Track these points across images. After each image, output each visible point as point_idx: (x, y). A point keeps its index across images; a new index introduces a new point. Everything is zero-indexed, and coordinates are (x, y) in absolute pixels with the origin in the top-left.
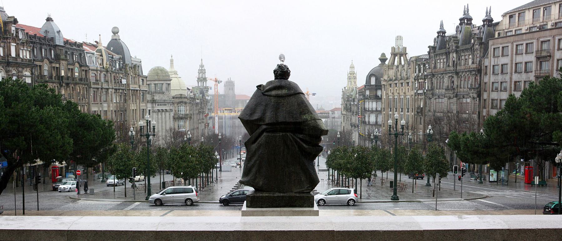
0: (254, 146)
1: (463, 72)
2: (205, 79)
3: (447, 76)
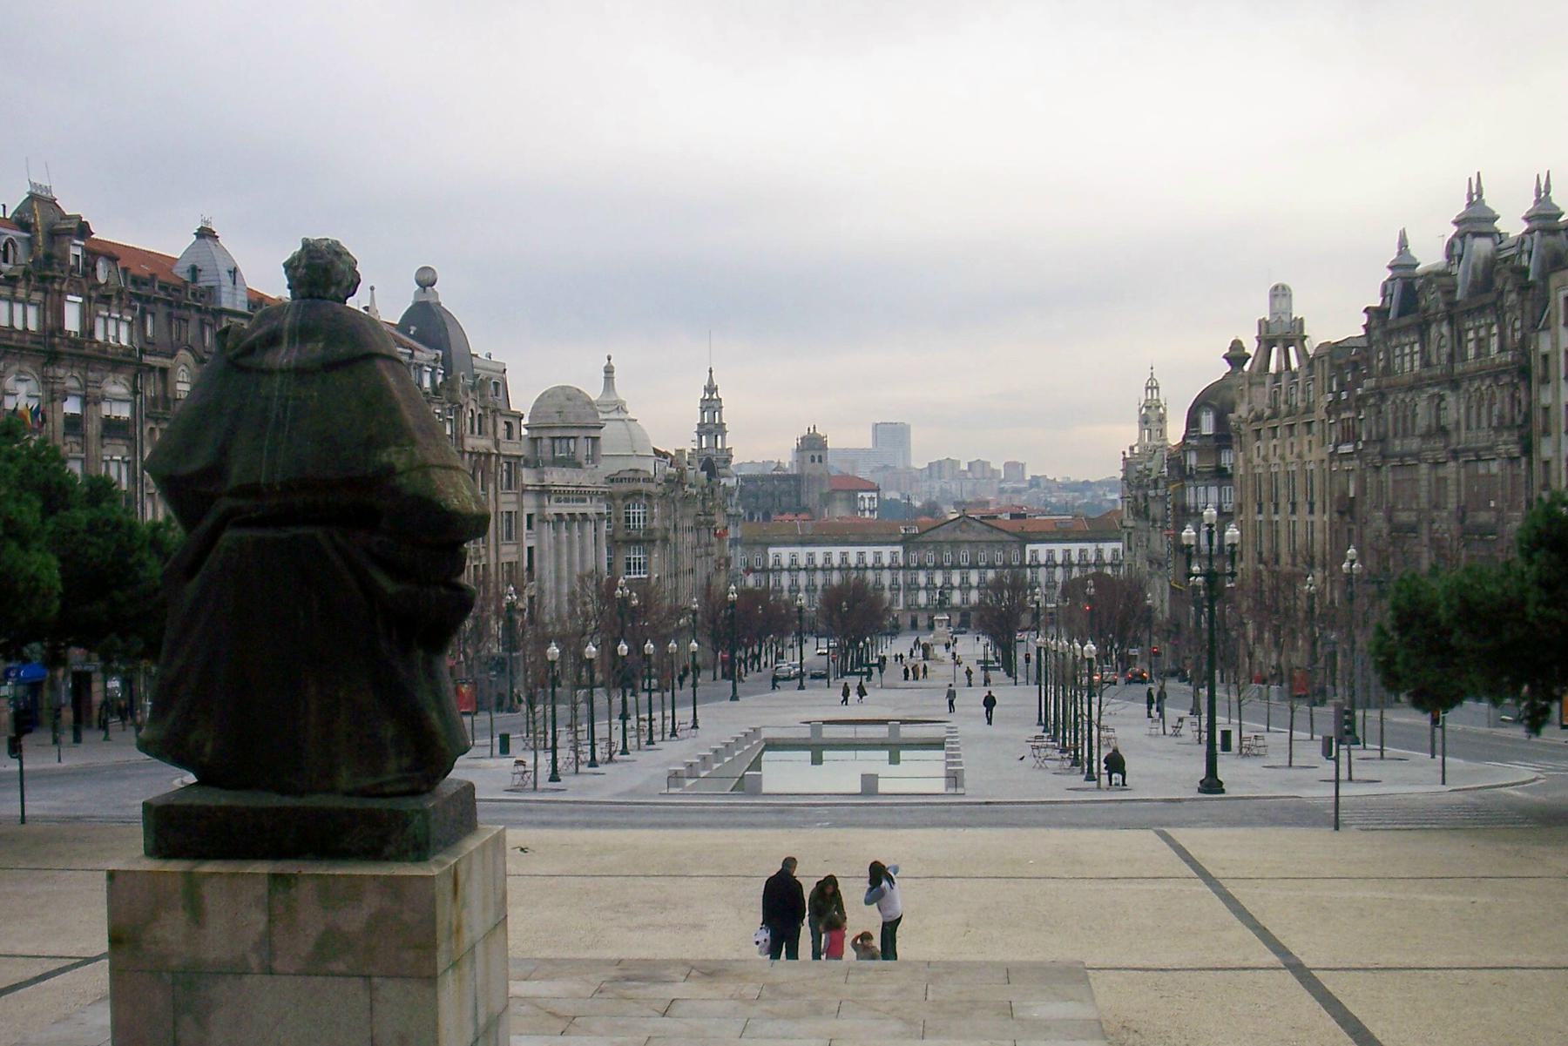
1: (1471, 380)
2: (720, 429)
3: (1425, 396)
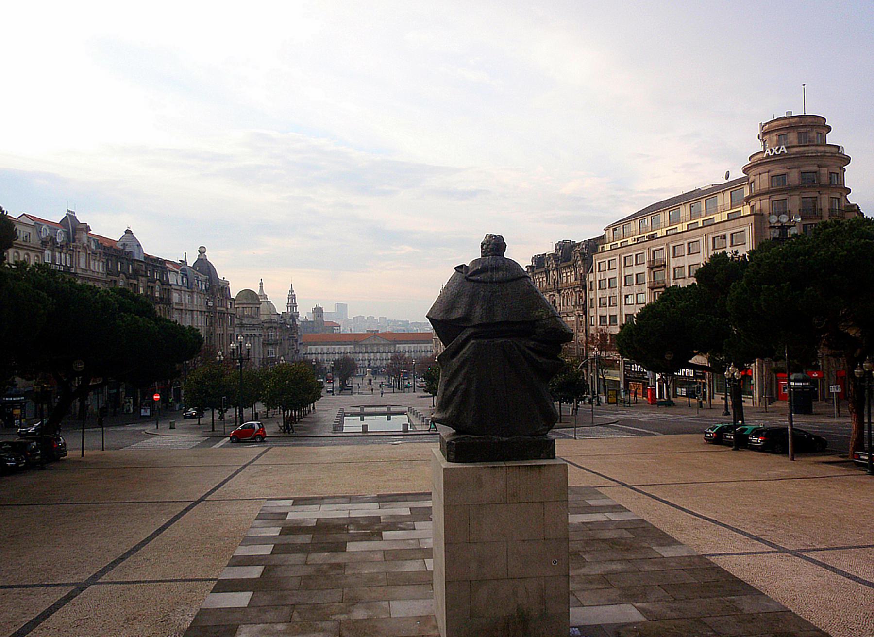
0: (455, 362)
